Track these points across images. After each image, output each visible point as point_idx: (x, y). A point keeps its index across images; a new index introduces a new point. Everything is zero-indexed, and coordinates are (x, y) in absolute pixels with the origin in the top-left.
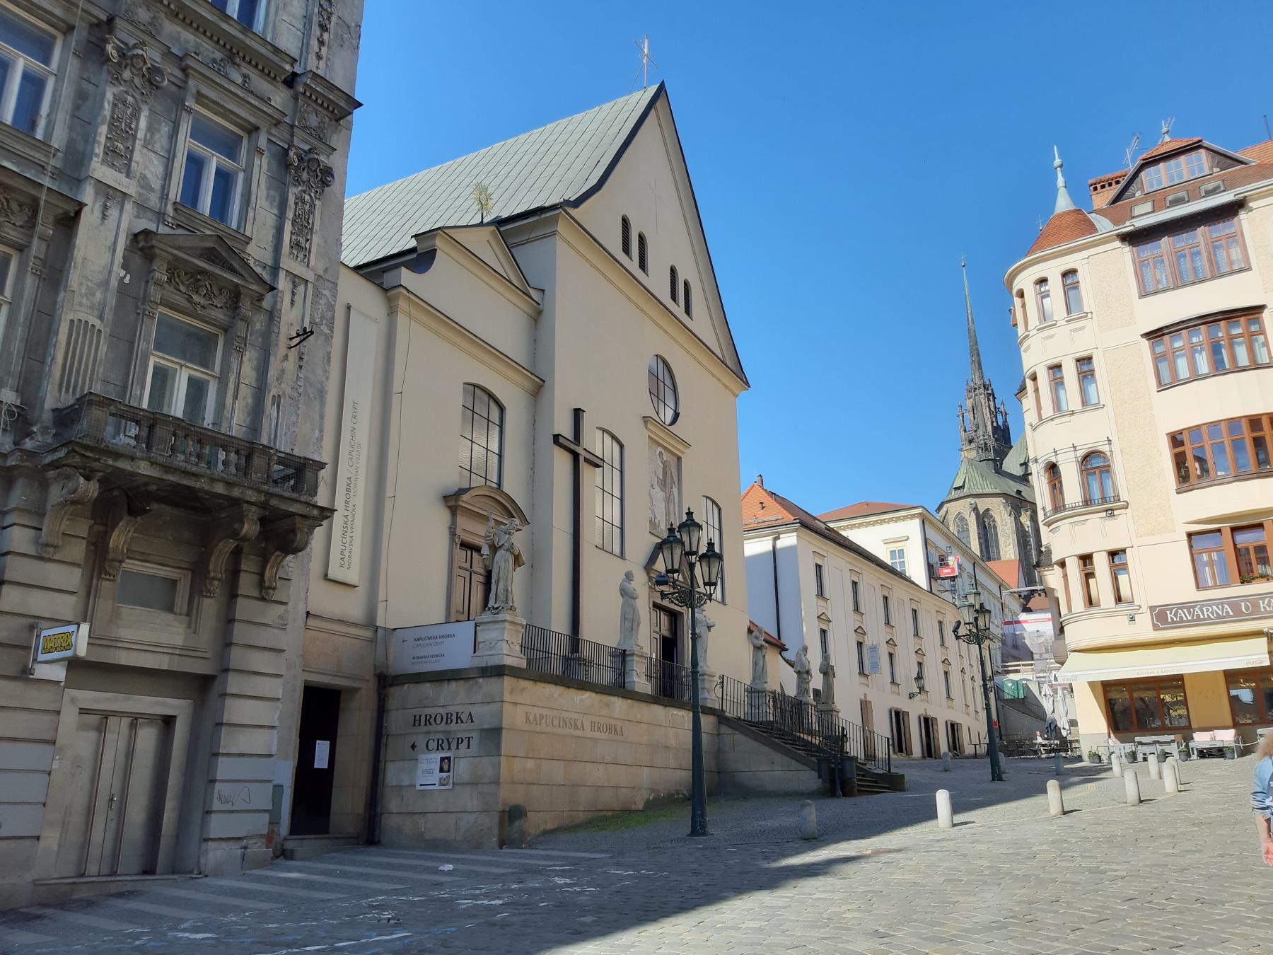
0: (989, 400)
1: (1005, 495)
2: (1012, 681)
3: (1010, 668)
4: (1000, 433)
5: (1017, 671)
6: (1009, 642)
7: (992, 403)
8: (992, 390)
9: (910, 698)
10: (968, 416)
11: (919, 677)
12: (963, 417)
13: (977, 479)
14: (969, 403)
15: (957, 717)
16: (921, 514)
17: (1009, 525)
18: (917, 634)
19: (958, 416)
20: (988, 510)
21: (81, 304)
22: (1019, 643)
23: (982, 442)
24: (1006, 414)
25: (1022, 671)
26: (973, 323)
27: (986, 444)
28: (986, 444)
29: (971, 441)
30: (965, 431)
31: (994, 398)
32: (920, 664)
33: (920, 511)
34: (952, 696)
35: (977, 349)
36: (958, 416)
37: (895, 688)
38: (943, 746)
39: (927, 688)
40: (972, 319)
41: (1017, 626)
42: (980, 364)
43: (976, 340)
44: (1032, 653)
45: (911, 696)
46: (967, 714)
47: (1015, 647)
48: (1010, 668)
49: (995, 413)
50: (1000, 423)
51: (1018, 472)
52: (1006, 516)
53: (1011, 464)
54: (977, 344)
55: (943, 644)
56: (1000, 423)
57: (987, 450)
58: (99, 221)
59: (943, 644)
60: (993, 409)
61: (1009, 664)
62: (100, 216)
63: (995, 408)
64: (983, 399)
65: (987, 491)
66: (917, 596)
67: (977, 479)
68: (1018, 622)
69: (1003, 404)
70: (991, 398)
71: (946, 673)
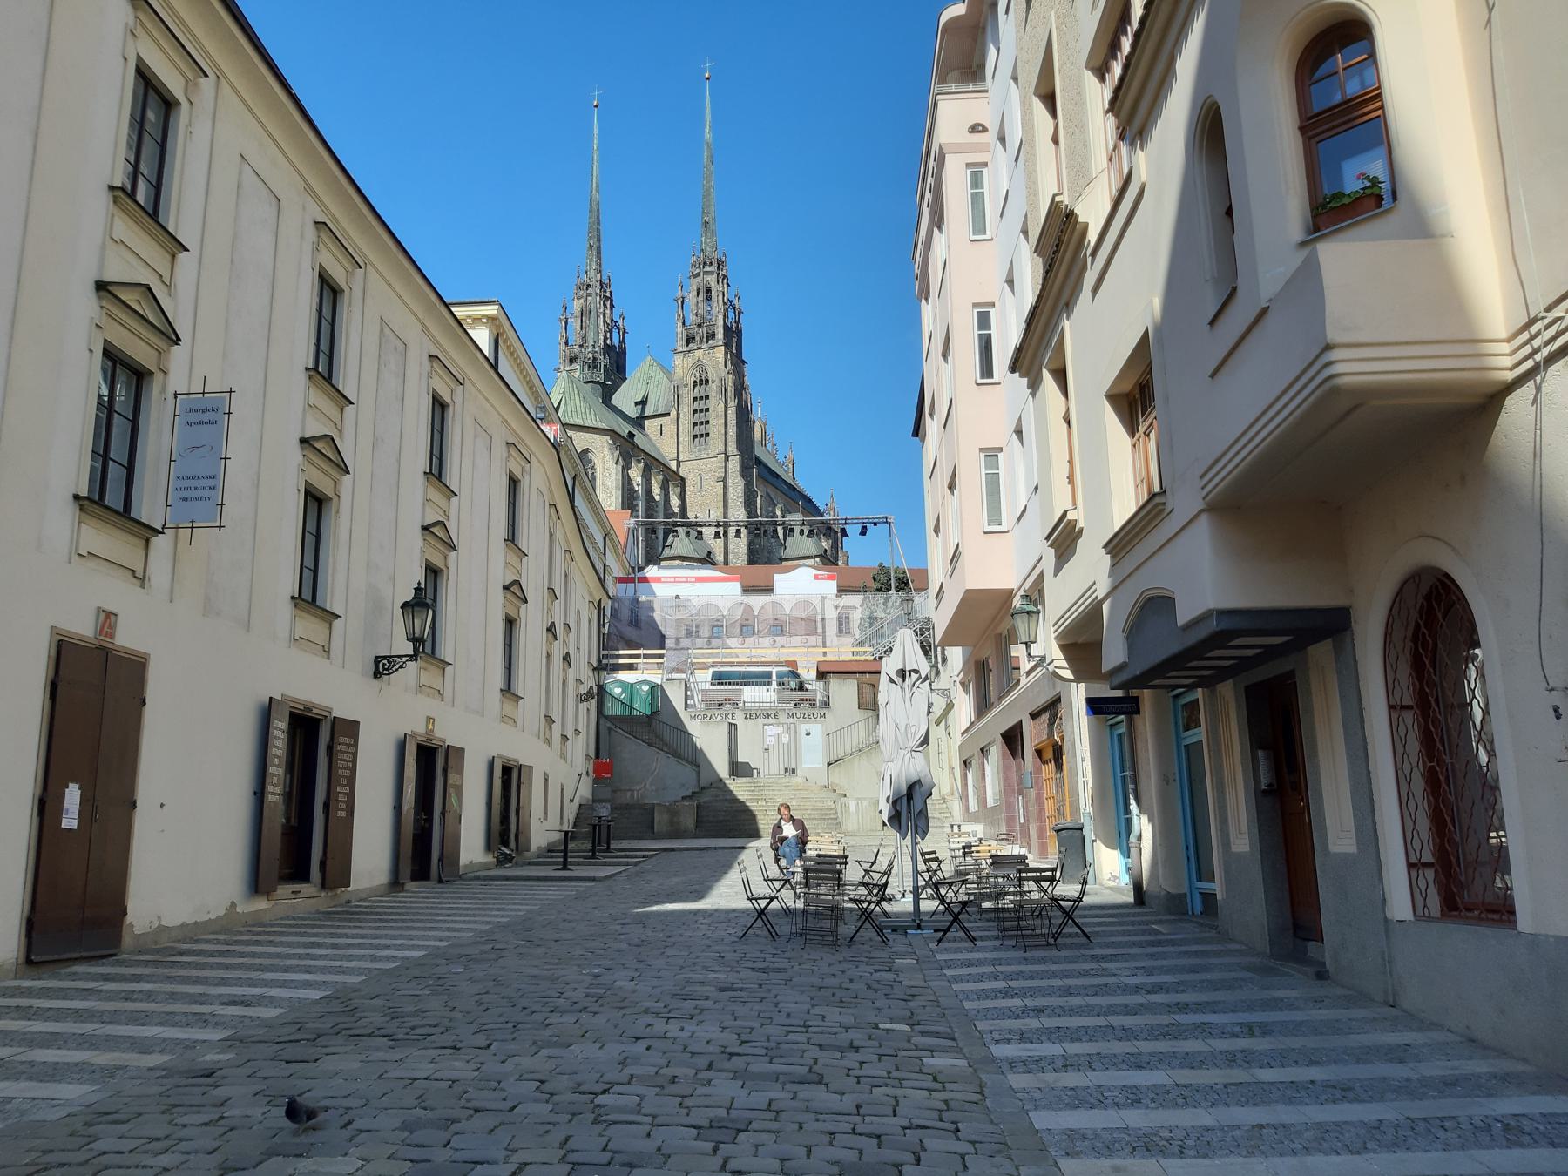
0: (605, 305)
1: (612, 433)
2: (623, 684)
3: (621, 661)
4: (614, 355)
5: (631, 667)
6: (625, 614)
7: (608, 312)
8: (611, 292)
9: (377, 674)
10: (575, 323)
11: (423, 602)
12: (566, 323)
13: (578, 404)
14: (577, 305)
15: (523, 748)
16: (492, 319)
17: (613, 475)
18: (436, 473)
19: (560, 320)
20: (587, 450)
22: (642, 616)
23: (590, 355)
24: (624, 332)
25: (641, 666)
26: (598, 191)
27: (595, 359)
28: (595, 359)
29: (572, 360)
30: (567, 344)
31: (612, 306)
32: (433, 572)
33: (492, 310)
34: (519, 689)
35: (598, 230)
36: (560, 320)
37: (309, 626)
38: (472, 847)
39: (446, 650)
40: (597, 186)
41: (641, 586)
42: (599, 252)
43: (598, 217)
44: (663, 637)
45: (382, 667)
46: (548, 741)
47: (635, 622)
48: (621, 661)
49: (612, 326)
50: (616, 341)
51: (633, 412)
52: (611, 464)
53: (625, 398)
54: (599, 223)
55: (512, 539)
56: (616, 341)
57: (595, 367)
59: (512, 539)
60: (609, 321)
61: (622, 652)
63: (612, 320)
64: (595, 301)
65: (589, 423)
66: (458, 360)
67: (578, 404)
68: (645, 580)
69: (622, 316)
70: (608, 304)
71: (510, 623)
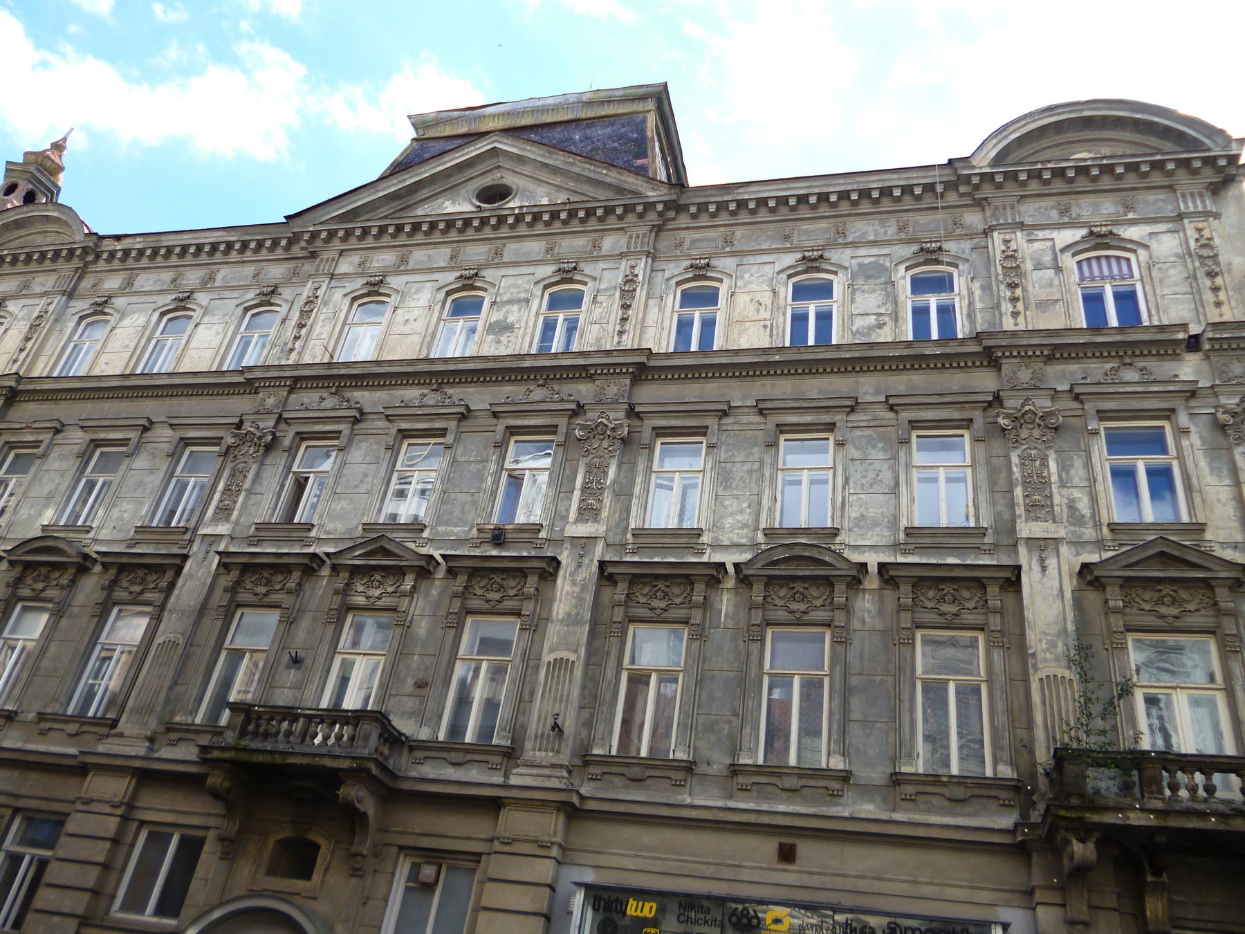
21: (1045, 660)
58: (1040, 575)
62: (1040, 569)
